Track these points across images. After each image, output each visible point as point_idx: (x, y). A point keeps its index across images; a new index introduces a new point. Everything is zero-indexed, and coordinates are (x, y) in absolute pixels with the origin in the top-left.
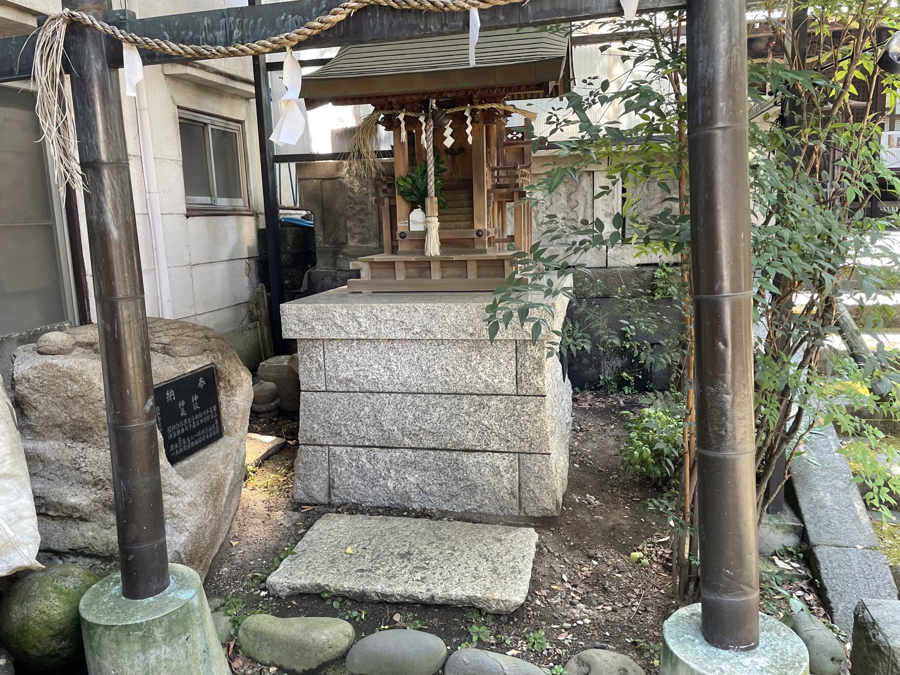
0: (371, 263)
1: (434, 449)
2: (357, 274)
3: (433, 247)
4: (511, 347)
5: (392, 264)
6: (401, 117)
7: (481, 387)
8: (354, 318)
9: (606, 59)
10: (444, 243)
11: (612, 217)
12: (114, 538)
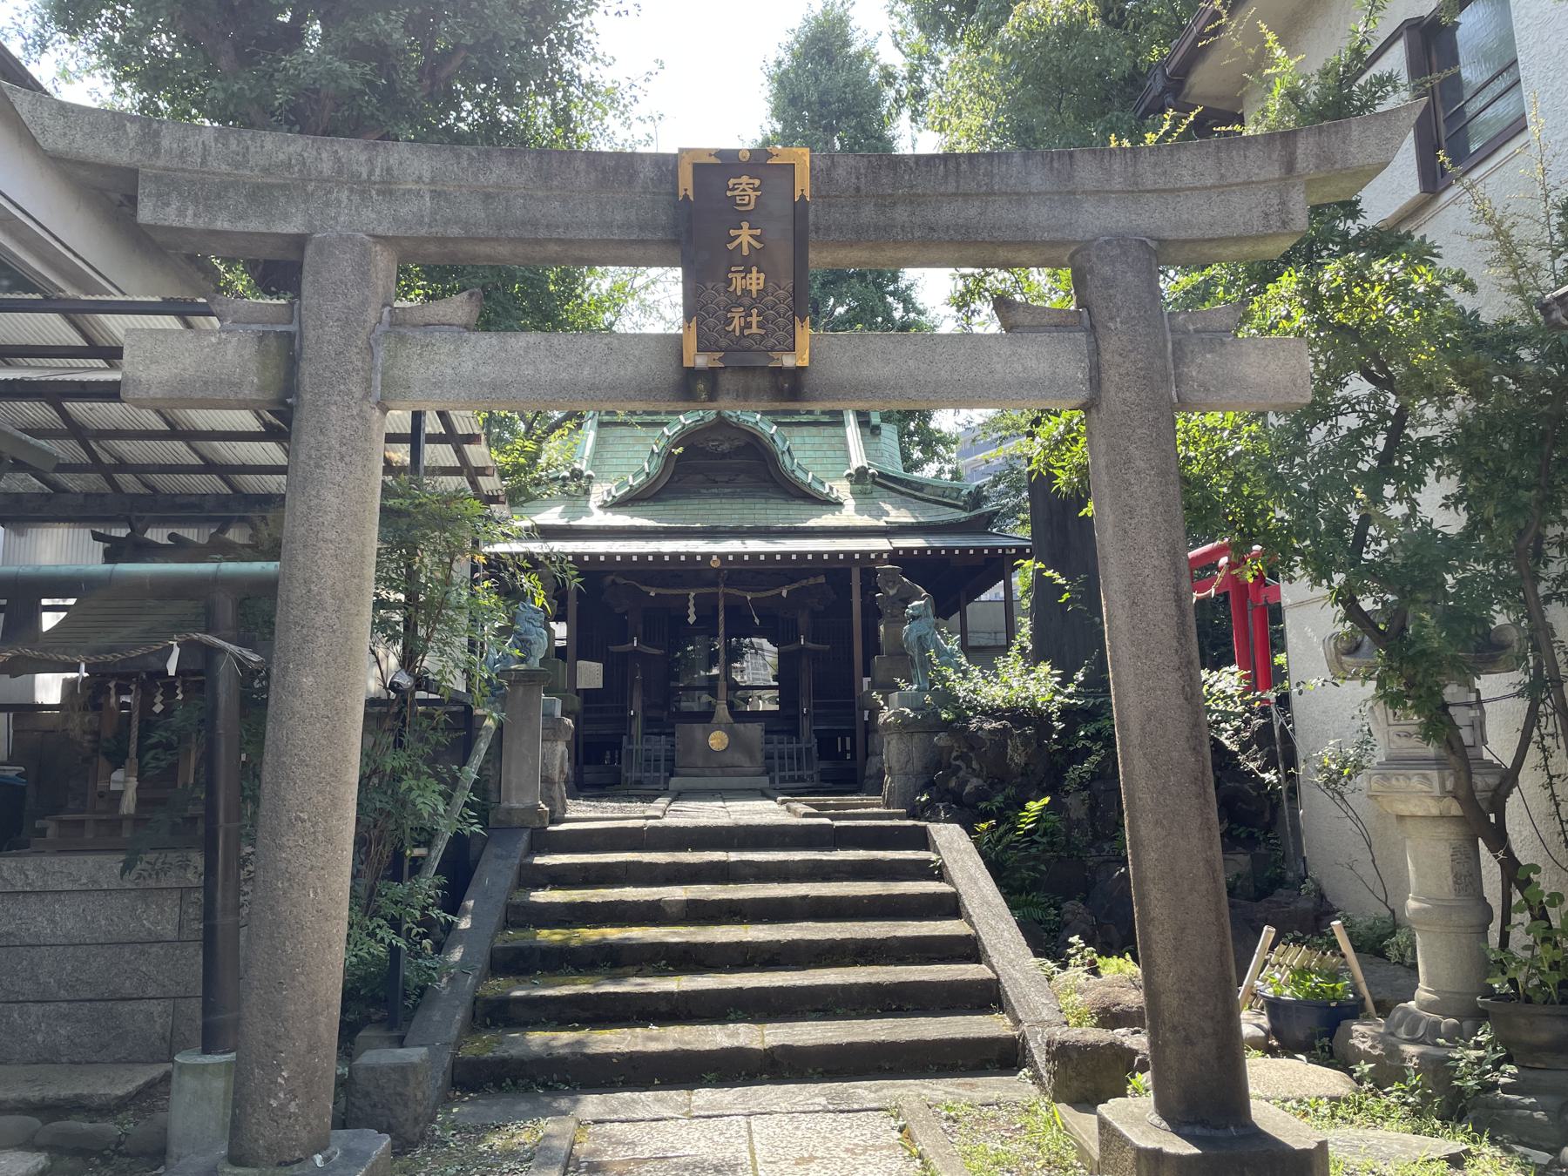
0: (61, 822)
1: (90, 1000)
2: (42, 832)
3: (128, 805)
4: (176, 895)
5: (81, 823)
6: (112, 685)
7: (143, 935)
8: (23, 872)
9: (1316, 65)
10: (140, 802)
11: (715, 720)
12: (408, 459)
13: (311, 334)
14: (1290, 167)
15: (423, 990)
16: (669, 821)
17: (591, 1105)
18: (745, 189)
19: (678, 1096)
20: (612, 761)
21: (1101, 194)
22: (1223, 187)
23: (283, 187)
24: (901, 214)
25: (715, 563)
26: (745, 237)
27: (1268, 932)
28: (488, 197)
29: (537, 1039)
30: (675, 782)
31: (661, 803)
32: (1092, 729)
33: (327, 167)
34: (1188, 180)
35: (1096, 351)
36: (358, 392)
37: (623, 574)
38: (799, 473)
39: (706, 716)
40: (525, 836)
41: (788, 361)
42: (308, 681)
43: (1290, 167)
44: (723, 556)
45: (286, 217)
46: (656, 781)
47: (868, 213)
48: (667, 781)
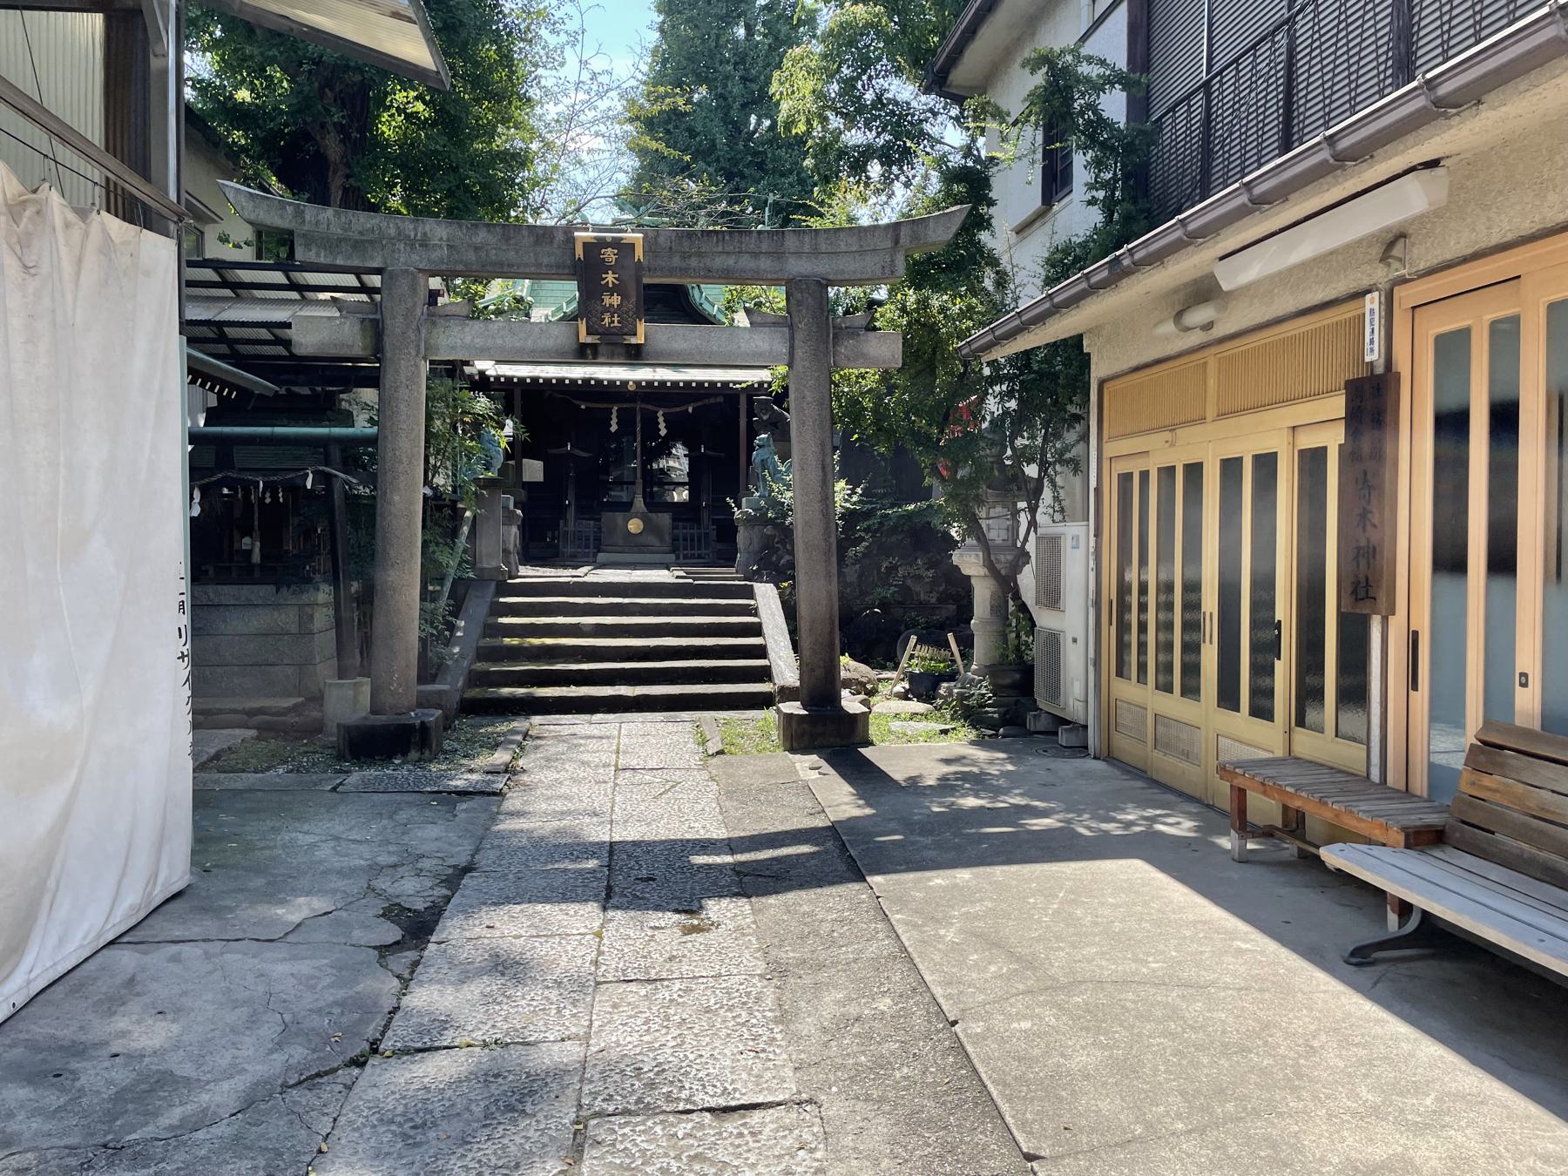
3: (256, 557)
10: (262, 556)
13: (388, 322)
14: (897, 242)
15: (440, 666)
16: (587, 579)
17: (537, 719)
18: (610, 255)
19: (587, 717)
20: (553, 539)
21: (798, 254)
22: (862, 252)
23: (370, 242)
24: (694, 262)
25: (631, 386)
26: (610, 278)
27: (914, 639)
28: (476, 249)
29: (506, 691)
30: (601, 557)
31: (585, 569)
32: (865, 524)
33: (392, 232)
34: (843, 248)
35: (792, 339)
36: (413, 353)
37: (561, 392)
38: (706, 306)
39: (626, 507)
40: (493, 585)
41: (633, 341)
42: (396, 498)
43: (897, 242)
44: (638, 383)
45: (372, 258)
46: (586, 555)
47: (676, 261)
48: (595, 556)
